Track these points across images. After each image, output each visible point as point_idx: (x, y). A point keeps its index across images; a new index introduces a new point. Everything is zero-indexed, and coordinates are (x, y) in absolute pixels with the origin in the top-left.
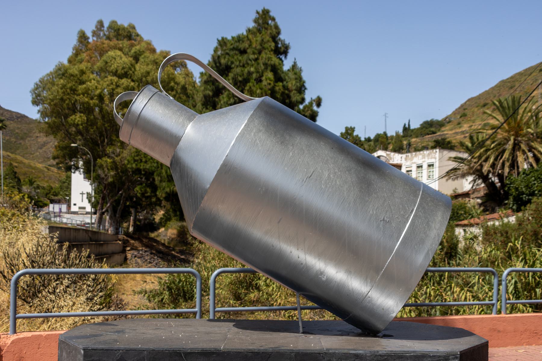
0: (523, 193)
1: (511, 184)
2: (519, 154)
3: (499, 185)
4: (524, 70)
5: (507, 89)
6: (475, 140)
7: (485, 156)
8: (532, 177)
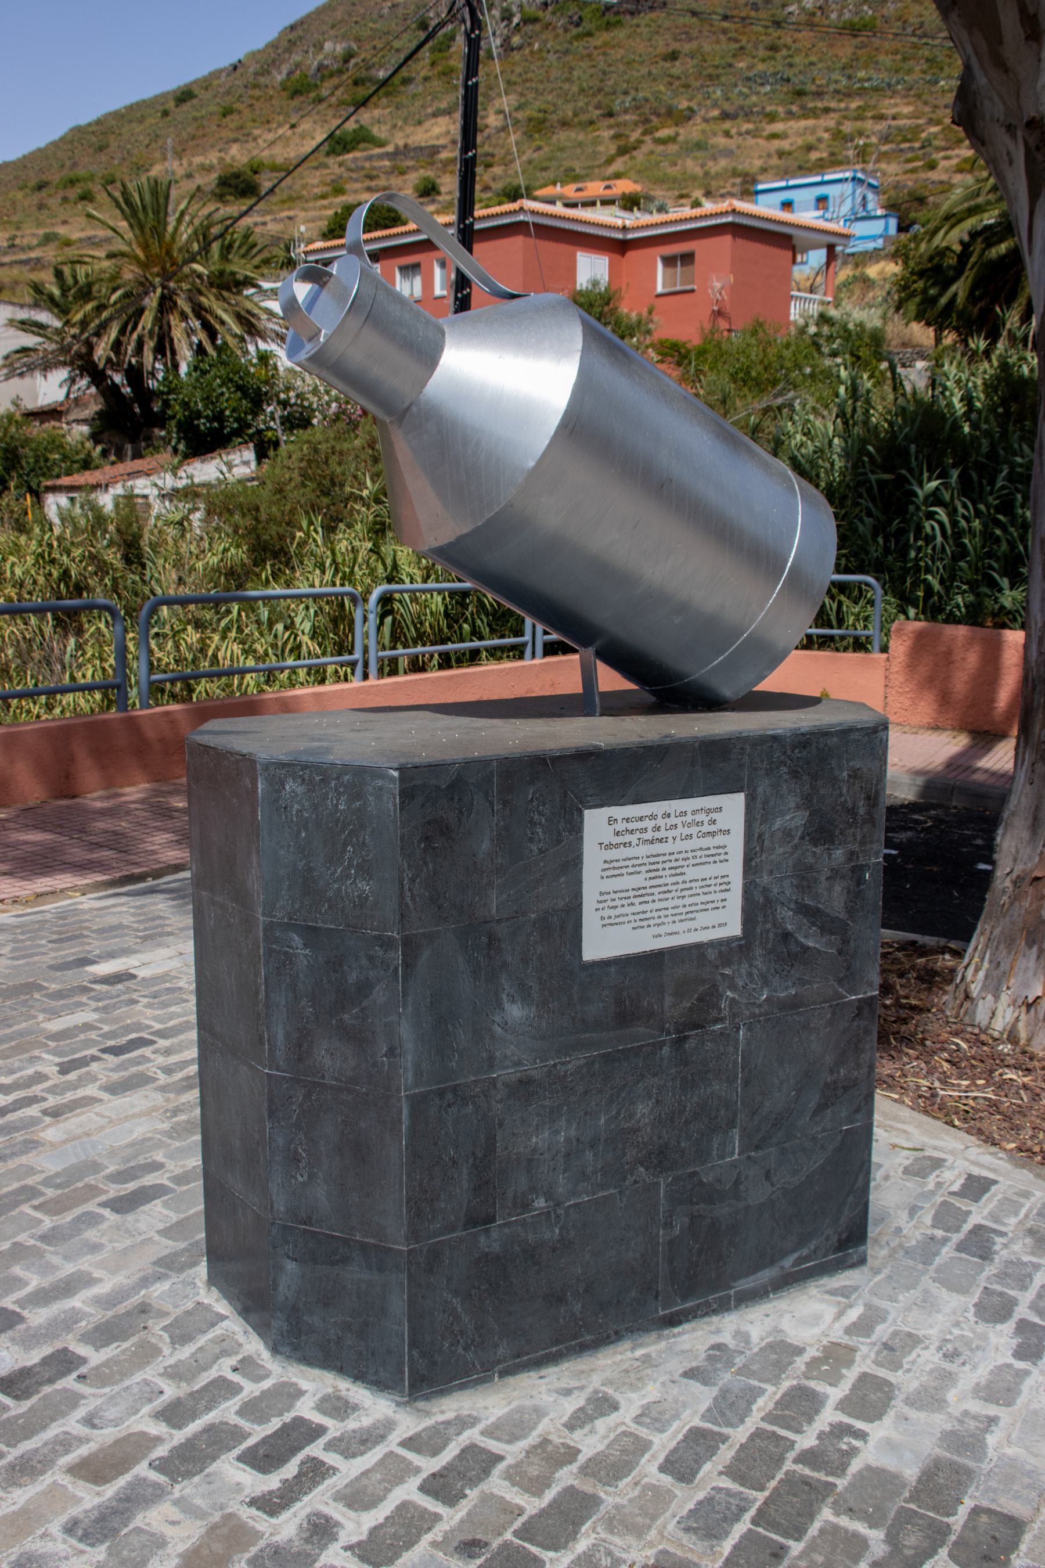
0: (199, 415)
1: (169, 393)
2: (174, 320)
3: (127, 390)
4: (125, 108)
5: (91, 151)
6: (70, 281)
7: (97, 322)
8: (216, 377)
